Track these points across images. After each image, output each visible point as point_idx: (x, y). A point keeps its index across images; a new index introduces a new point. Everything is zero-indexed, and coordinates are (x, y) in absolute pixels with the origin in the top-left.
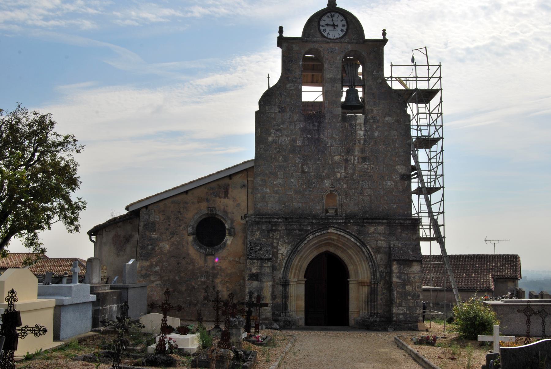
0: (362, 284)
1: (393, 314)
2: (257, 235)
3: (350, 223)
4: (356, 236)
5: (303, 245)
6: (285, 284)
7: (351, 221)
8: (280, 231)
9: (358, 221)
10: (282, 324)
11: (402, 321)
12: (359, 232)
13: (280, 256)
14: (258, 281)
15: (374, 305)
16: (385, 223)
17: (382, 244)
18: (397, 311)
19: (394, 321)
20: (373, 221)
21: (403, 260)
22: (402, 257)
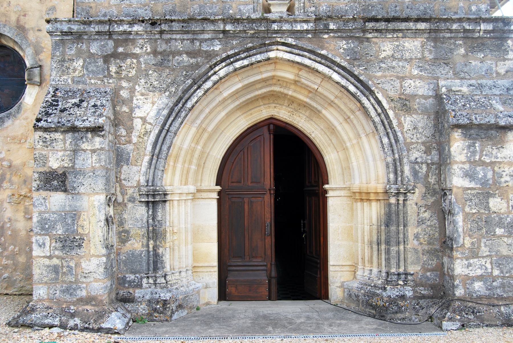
0: (363, 197)
1: (452, 278)
2: (75, 70)
3: (328, 31)
4: (344, 68)
5: (200, 93)
6: (155, 199)
7: (332, 26)
8: (136, 56)
9: (351, 26)
10: (142, 309)
11: (480, 297)
12: (355, 57)
13: (137, 123)
14: (65, 191)
15: (398, 252)
16: (423, 31)
17: (419, 88)
18: (466, 271)
19: (459, 299)
20: (391, 26)
21: (480, 126)
22: (477, 119)
